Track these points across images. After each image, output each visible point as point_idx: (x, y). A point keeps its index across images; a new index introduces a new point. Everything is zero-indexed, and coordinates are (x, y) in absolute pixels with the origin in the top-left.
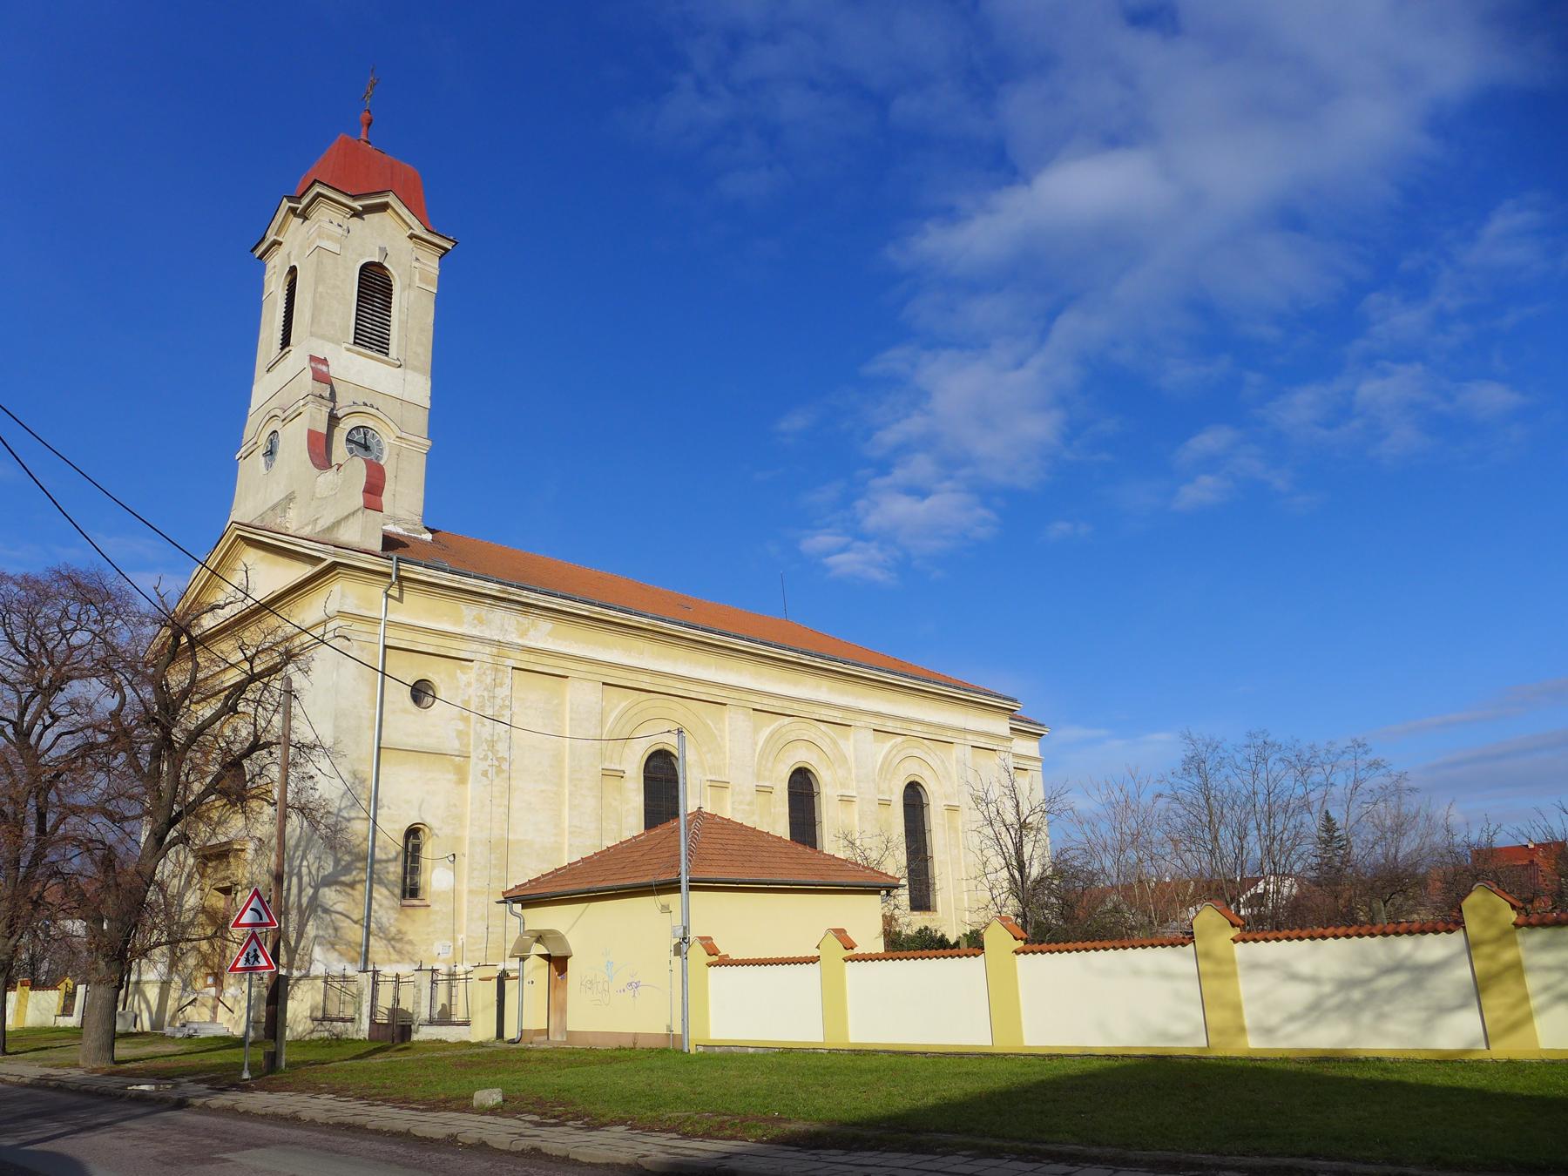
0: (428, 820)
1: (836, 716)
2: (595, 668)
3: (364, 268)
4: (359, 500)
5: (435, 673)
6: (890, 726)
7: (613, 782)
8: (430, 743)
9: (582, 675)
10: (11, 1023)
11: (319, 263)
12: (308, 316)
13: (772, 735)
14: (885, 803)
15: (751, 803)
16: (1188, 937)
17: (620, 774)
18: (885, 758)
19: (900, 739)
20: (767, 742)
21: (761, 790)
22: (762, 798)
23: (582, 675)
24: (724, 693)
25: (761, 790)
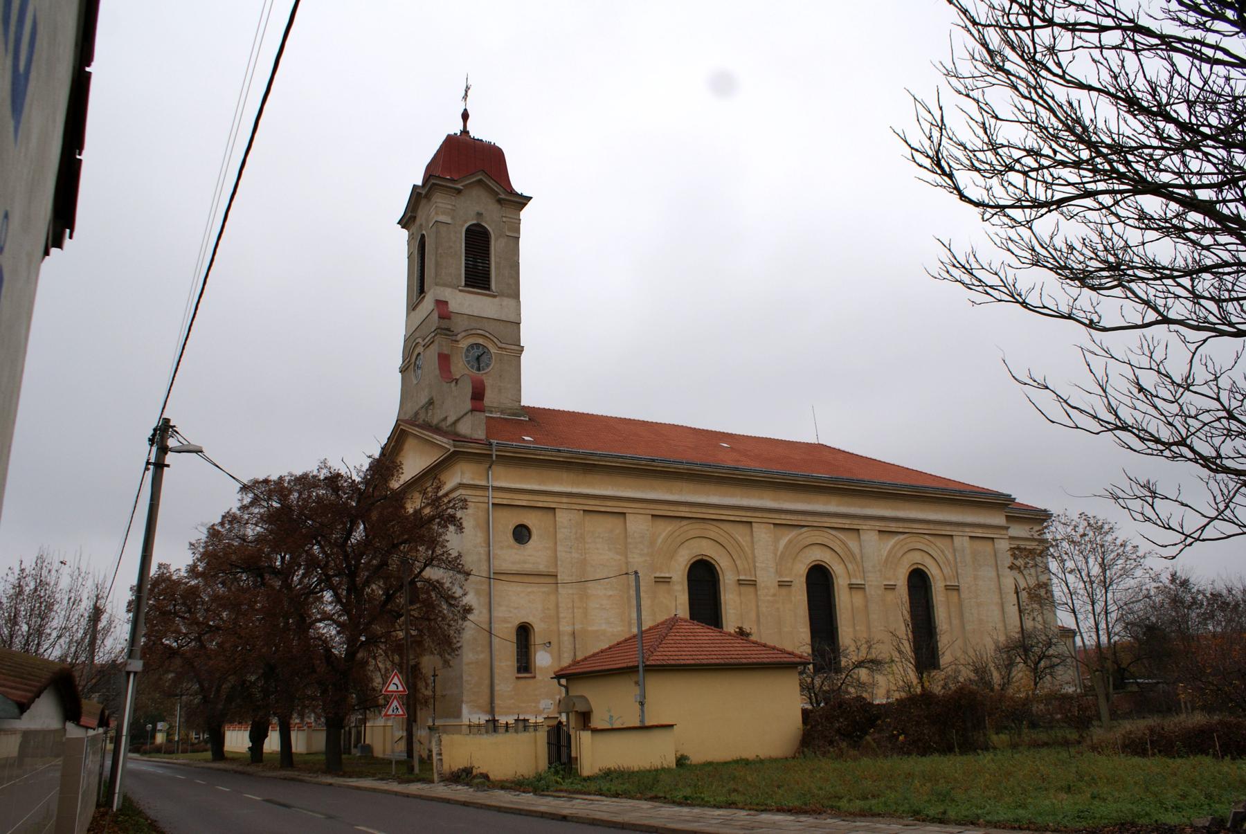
0: (530, 619)
1: (846, 523)
2: (644, 505)
3: (468, 230)
4: (468, 405)
5: (530, 520)
6: (893, 526)
7: (663, 587)
8: (528, 567)
9: (565, 506)
10: (294, 750)
11: (438, 232)
12: (433, 271)
13: (790, 542)
14: (891, 588)
15: (774, 595)
16: (245, 488)
17: (666, 581)
18: (890, 552)
19: (902, 537)
20: (786, 547)
21: (782, 584)
22: (784, 591)
23: (565, 506)
24: (749, 514)
25: (782, 584)
